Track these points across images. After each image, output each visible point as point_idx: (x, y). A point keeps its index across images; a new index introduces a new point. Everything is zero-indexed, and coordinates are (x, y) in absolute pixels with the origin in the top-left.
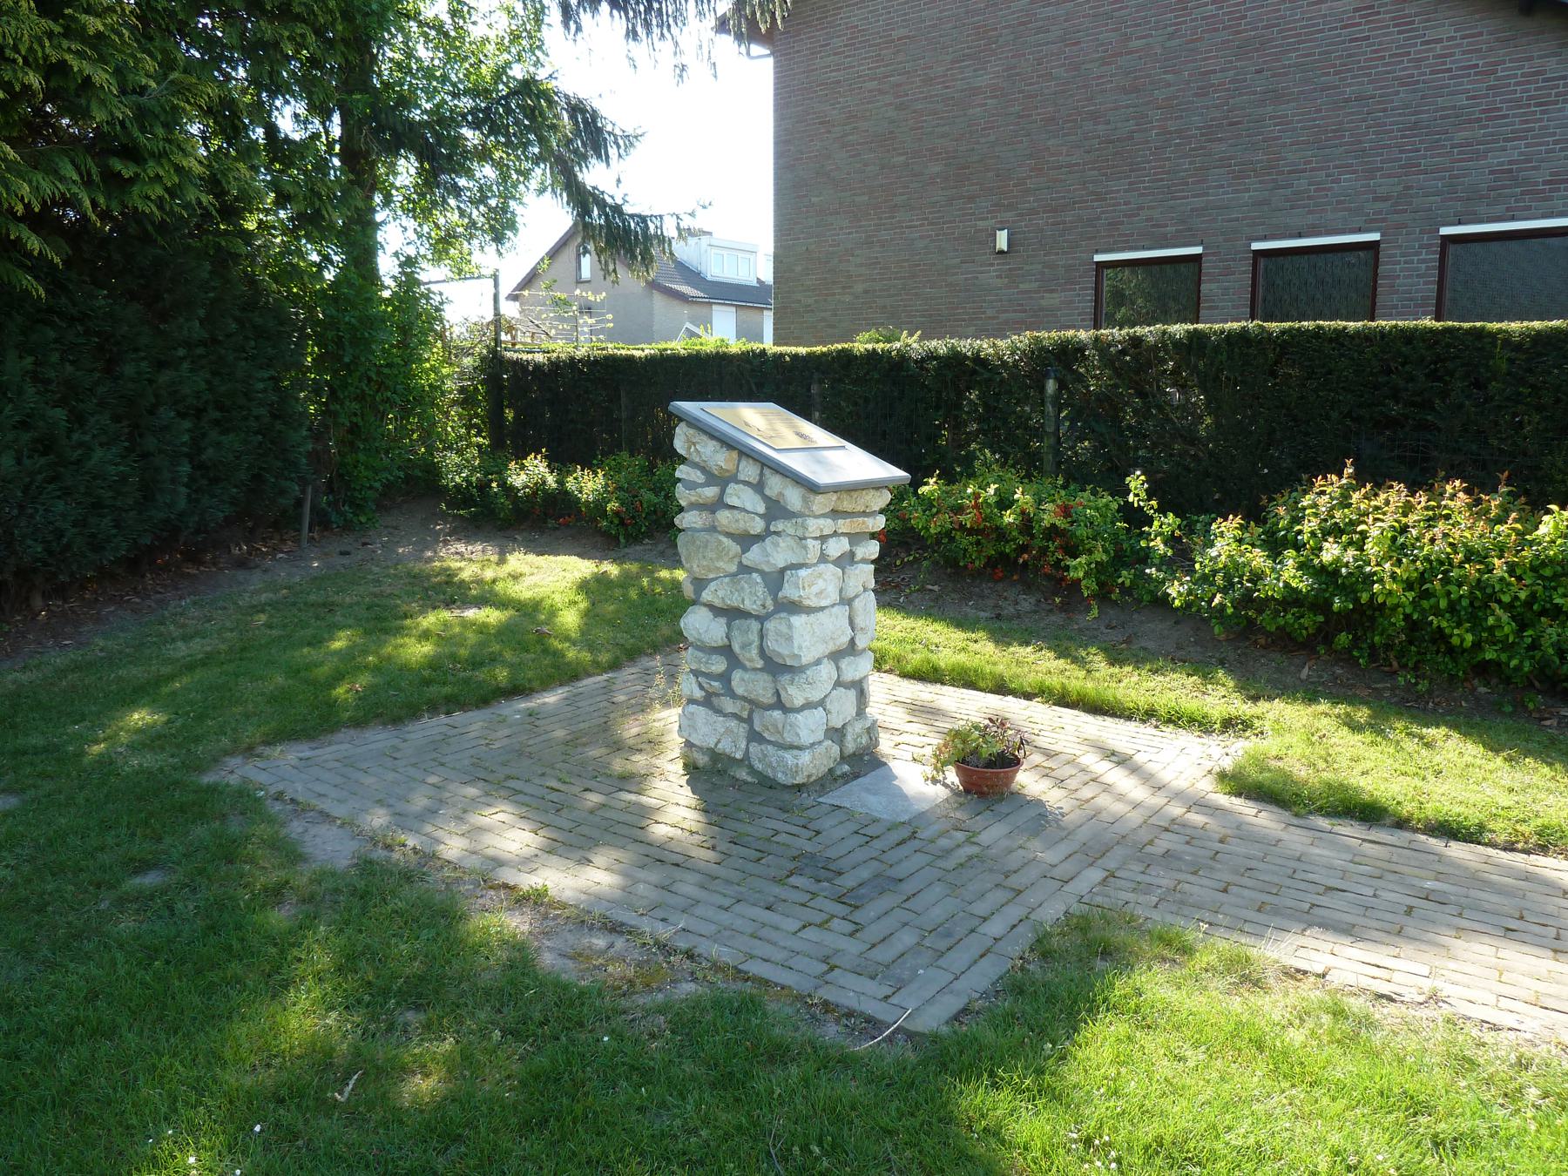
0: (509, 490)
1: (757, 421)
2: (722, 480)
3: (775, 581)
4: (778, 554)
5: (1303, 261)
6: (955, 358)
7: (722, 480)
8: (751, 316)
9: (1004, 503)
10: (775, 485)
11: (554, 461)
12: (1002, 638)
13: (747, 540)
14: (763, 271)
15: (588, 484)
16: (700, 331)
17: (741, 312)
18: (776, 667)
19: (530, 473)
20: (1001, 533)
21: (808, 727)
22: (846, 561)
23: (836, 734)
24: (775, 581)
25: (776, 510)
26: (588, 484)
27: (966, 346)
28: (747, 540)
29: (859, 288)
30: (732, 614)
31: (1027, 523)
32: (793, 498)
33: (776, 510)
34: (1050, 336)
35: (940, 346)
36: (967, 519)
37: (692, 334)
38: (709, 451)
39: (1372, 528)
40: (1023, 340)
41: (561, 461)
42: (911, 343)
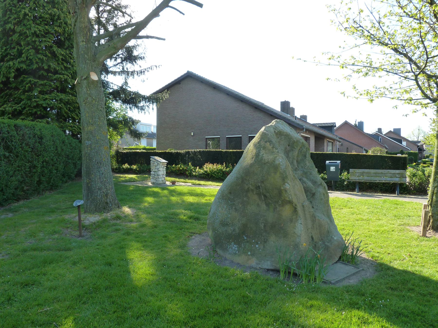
0: (123, 168)
1: (157, 158)
2: (154, 162)
3: (158, 169)
4: (158, 167)
5: (235, 139)
6: (177, 152)
7: (154, 162)
8: (150, 140)
9: (181, 167)
10: (158, 162)
11: (129, 164)
12: (179, 179)
13: (156, 166)
14: (154, 130)
15: (134, 167)
16: (139, 144)
17: (148, 139)
18: (158, 175)
19: (126, 166)
20: (181, 170)
21: (160, 180)
22: (163, 168)
23: (163, 181)
24: (158, 169)
25: (158, 164)
26: (134, 167)
27: (179, 151)
28: (156, 166)
29: (171, 140)
30: (155, 172)
31: (183, 169)
32: (159, 163)
33: (158, 164)
34: (187, 150)
35: (176, 151)
36: (177, 169)
37: (137, 145)
38: (153, 160)
39: (209, 167)
40: (184, 151)
41: (130, 164)
42: (173, 151)
